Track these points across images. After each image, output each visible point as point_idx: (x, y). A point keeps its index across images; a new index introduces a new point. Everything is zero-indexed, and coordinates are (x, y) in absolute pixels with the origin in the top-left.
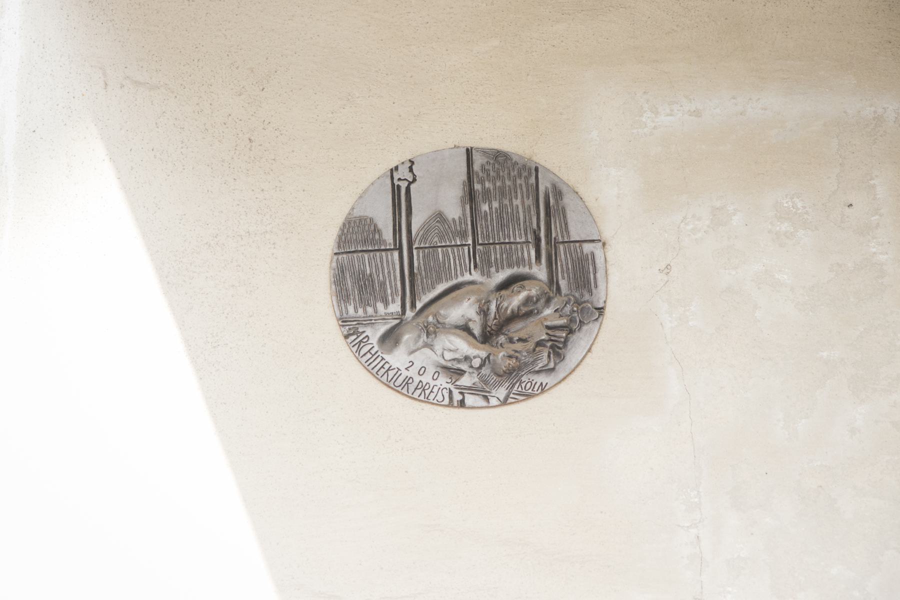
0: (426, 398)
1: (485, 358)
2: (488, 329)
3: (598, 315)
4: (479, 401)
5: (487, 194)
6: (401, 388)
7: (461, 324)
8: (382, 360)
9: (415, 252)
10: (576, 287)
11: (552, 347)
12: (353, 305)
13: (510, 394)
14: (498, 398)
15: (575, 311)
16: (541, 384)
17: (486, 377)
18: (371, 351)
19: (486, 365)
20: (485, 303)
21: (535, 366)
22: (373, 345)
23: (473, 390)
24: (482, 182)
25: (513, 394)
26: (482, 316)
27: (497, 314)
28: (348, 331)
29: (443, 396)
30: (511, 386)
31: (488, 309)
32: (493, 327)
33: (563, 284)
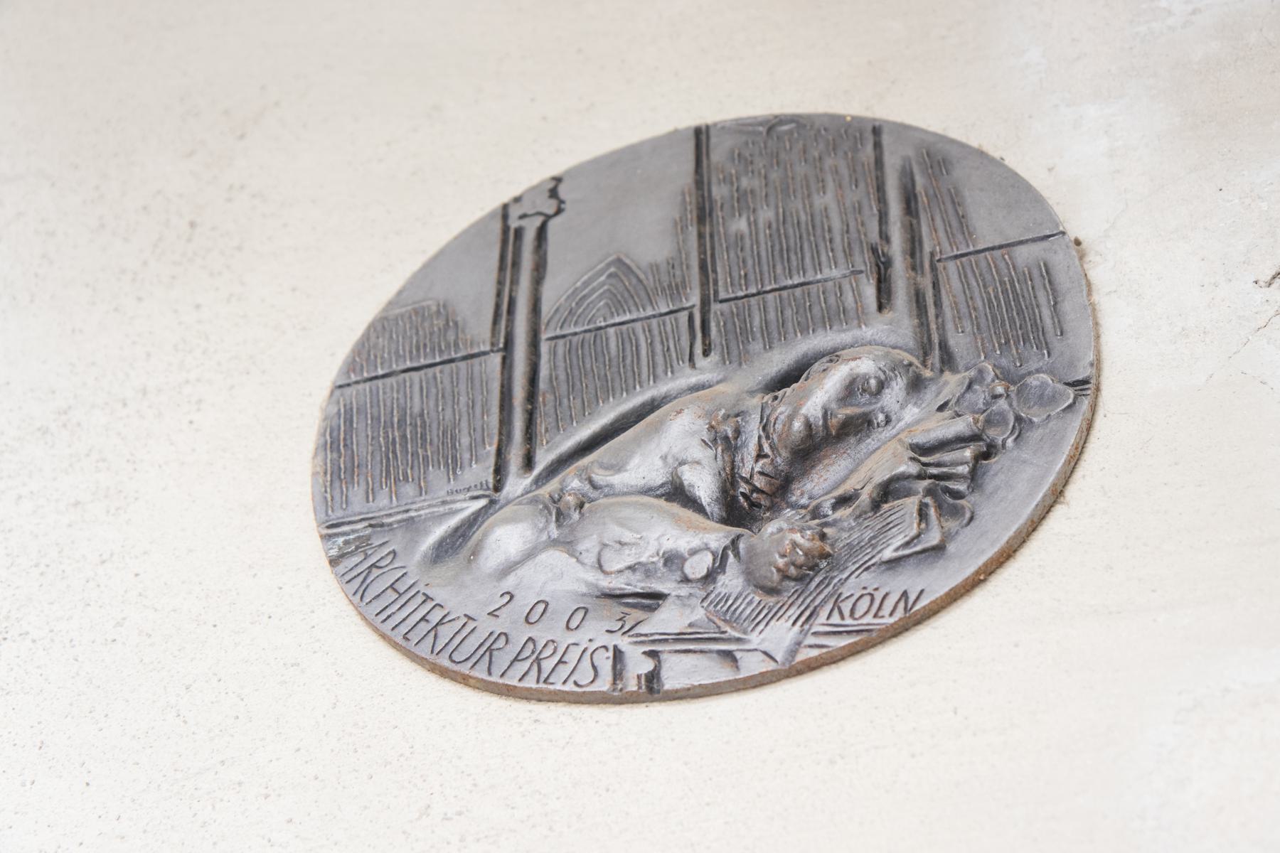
0: (542, 679)
1: (725, 549)
2: (743, 488)
3: (1072, 396)
4: (708, 671)
5: (743, 201)
6: (470, 664)
7: (659, 481)
8: (424, 602)
9: (544, 348)
10: (1000, 345)
11: (929, 492)
12: (365, 487)
13: (806, 635)
14: (765, 653)
15: (1001, 396)
16: (905, 594)
17: (730, 602)
18: (396, 586)
19: (728, 569)
20: (726, 417)
21: (879, 548)
22: (404, 571)
23: (686, 640)
24: (728, 180)
25: (815, 634)
26: (720, 449)
27: (764, 440)
28: (340, 549)
29: (594, 667)
30: (807, 613)
31: (738, 432)
32: (759, 482)
33: (959, 342)
